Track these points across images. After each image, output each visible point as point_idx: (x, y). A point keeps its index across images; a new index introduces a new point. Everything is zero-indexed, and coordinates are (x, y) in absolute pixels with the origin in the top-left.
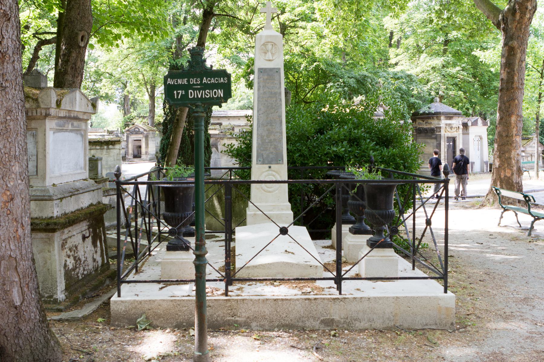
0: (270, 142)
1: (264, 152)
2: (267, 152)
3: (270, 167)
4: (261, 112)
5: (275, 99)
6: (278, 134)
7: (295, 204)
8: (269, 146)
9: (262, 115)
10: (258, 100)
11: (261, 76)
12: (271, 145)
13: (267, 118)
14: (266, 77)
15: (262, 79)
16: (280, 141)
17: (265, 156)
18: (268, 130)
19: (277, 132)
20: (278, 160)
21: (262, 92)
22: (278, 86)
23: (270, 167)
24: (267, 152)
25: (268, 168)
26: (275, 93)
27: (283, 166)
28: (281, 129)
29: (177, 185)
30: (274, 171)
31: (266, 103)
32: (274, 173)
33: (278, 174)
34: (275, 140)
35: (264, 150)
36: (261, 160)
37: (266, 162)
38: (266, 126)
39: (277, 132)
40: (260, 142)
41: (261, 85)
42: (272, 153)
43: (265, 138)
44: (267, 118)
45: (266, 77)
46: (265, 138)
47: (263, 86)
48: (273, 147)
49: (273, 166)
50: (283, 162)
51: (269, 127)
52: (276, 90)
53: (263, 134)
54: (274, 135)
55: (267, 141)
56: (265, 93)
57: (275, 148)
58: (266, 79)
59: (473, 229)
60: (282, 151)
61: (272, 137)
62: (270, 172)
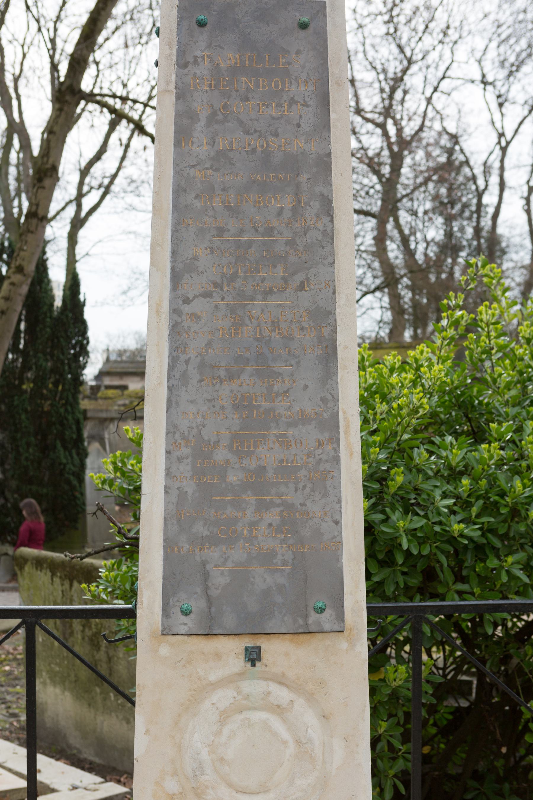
0: (257, 481)
1: (213, 554)
2: (238, 554)
3: (253, 656)
4: (193, 285)
5: (287, 201)
6: (310, 434)
7: (57, 371)
8: (250, 515)
9: (200, 306)
10: (176, 207)
11: (199, 49)
12: (263, 506)
13: (238, 325)
14: (229, 57)
15: (203, 69)
16: (325, 478)
17: (219, 580)
18: (243, 404)
19: (303, 419)
20: (307, 614)
21: (201, 149)
22: (308, 117)
23: (253, 656)
24: (238, 554)
25: (237, 663)
26: (293, 164)
27: (341, 643)
28: (330, 400)
29: (13, 95)
30: (281, 681)
31: (232, 225)
32: (282, 695)
33: (310, 698)
34: (288, 470)
35: (213, 541)
36: (198, 604)
37: (229, 621)
38: (232, 376)
39: (303, 419)
40: (190, 487)
41: (200, 104)
42: (267, 558)
43: (221, 455)
44: (238, 325)
45: (229, 57)
46: (221, 455)
47: (212, 119)
48: (272, 516)
49: (273, 649)
50: (340, 617)
51: (248, 383)
52: (299, 145)
53: (208, 434)
54: (283, 440)
55: (233, 477)
56: (221, 159)
57: (290, 524)
58: (234, 71)
59: (359, 427)
60: (337, 543)
61: (269, 455)
62: (254, 687)
